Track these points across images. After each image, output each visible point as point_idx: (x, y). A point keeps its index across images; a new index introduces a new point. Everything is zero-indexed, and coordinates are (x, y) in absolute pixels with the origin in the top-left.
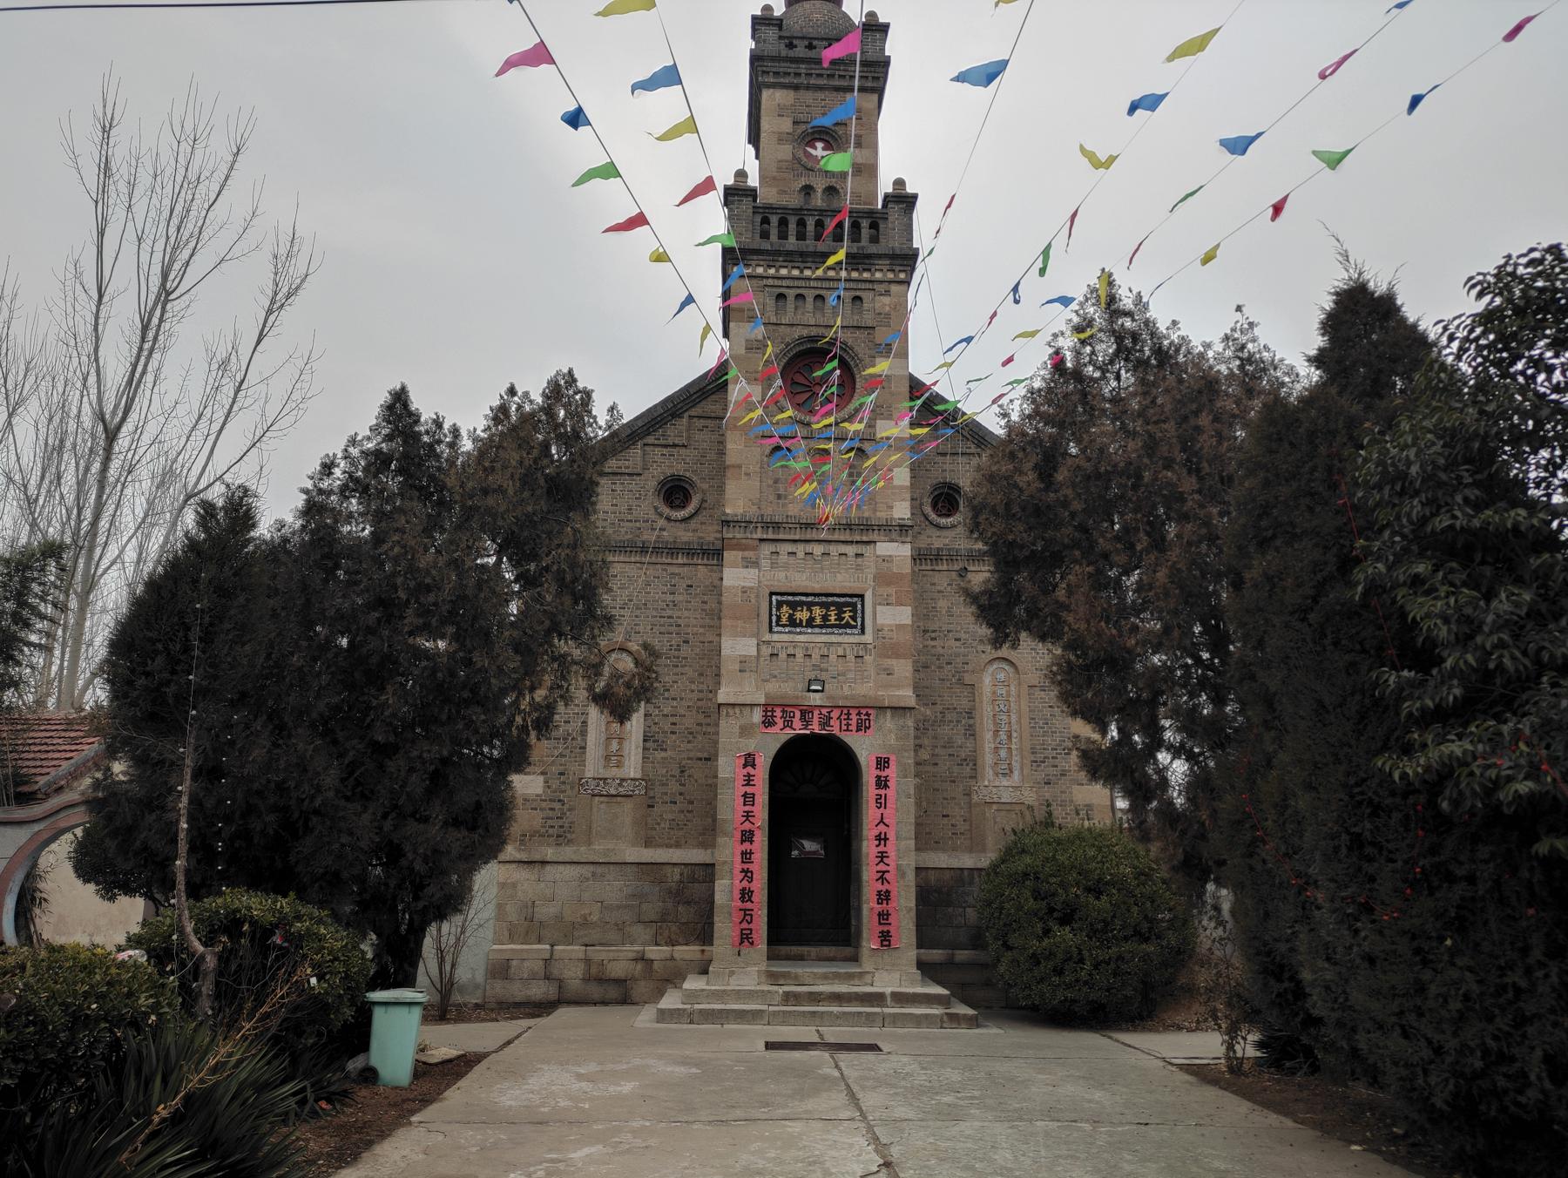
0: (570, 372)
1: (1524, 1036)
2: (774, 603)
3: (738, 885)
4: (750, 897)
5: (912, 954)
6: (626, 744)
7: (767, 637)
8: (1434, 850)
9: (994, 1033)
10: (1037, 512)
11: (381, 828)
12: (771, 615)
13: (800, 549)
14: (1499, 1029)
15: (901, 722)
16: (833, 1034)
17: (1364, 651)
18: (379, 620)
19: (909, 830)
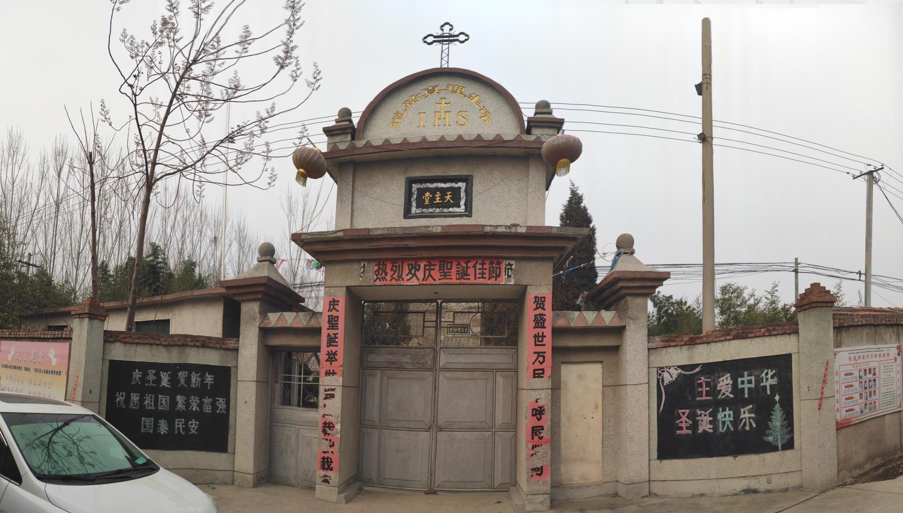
7: (447, 335)
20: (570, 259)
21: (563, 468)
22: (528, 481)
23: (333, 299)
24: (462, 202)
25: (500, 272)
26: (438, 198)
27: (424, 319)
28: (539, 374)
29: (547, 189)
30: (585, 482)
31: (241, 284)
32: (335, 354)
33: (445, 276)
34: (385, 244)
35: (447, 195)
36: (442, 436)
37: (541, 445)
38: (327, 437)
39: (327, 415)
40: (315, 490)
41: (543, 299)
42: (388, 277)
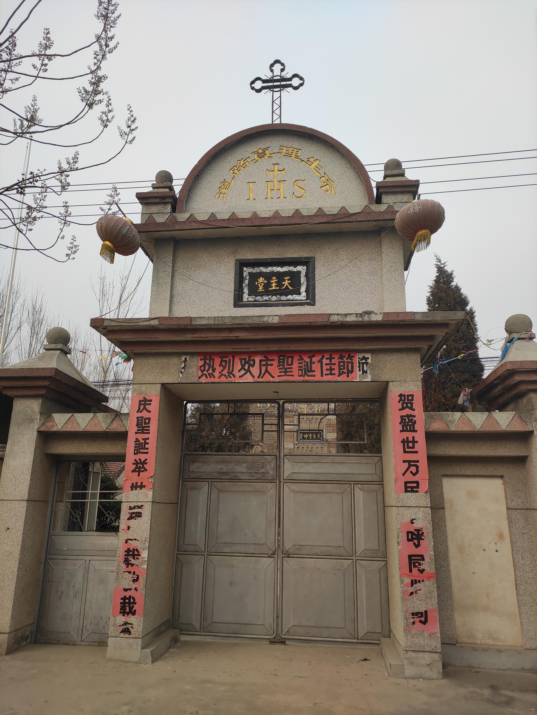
20: (442, 349)
21: (458, 619)
22: (407, 630)
23: (144, 398)
24: (303, 289)
25: (352, 367)
26: (274, 285)
27: (263, 422)
28: (412, 488)
29: (406, 269)
30: (494, 643)
31: (15, 375)
32: (145, 462)
33: (286, 372)
34: (211, 336)
35: (284, 281)
36: (290, 564)
37: (423, 581)
38: (130, 569)
39: (132, 540)
40: (107, 646)
41: (410, 398)
42: (216, 374)
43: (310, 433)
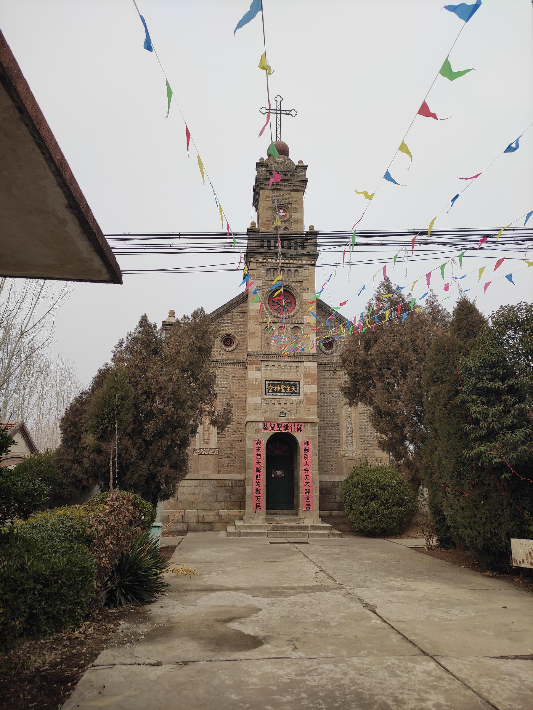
0: (202, 308)
1: (501, 528)
2: (267, 384)
3: (255, 488)
4: (259, 492)
5: (318, 512)
6: (211, 435)
7: (265, 397)
8: (479, 476)
9: (347, 539)
10: (365, 363)
11: (149, 469)
12: (266, 389)
13: (276, 364)
14: (495, 526)
15: (313, 428)
16: (291, 540)
17: (462, 418)
18: (146, 399)
19: (317, 467)
43: (282, 384)
